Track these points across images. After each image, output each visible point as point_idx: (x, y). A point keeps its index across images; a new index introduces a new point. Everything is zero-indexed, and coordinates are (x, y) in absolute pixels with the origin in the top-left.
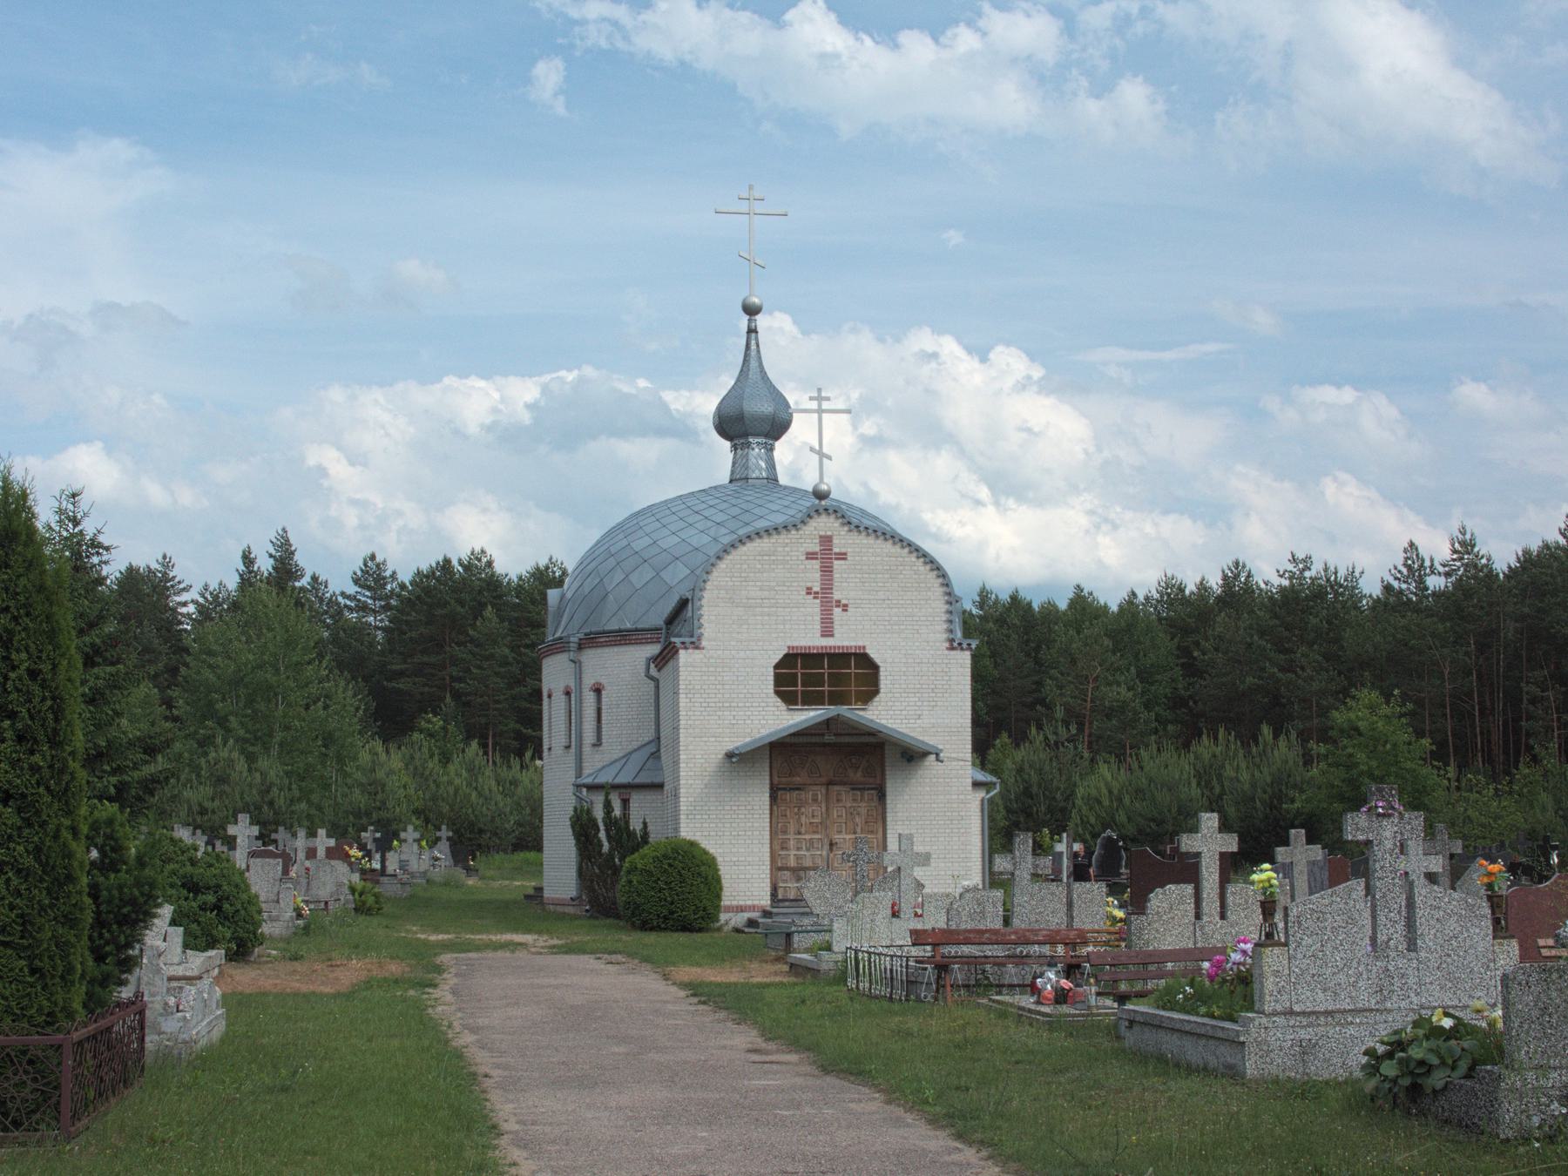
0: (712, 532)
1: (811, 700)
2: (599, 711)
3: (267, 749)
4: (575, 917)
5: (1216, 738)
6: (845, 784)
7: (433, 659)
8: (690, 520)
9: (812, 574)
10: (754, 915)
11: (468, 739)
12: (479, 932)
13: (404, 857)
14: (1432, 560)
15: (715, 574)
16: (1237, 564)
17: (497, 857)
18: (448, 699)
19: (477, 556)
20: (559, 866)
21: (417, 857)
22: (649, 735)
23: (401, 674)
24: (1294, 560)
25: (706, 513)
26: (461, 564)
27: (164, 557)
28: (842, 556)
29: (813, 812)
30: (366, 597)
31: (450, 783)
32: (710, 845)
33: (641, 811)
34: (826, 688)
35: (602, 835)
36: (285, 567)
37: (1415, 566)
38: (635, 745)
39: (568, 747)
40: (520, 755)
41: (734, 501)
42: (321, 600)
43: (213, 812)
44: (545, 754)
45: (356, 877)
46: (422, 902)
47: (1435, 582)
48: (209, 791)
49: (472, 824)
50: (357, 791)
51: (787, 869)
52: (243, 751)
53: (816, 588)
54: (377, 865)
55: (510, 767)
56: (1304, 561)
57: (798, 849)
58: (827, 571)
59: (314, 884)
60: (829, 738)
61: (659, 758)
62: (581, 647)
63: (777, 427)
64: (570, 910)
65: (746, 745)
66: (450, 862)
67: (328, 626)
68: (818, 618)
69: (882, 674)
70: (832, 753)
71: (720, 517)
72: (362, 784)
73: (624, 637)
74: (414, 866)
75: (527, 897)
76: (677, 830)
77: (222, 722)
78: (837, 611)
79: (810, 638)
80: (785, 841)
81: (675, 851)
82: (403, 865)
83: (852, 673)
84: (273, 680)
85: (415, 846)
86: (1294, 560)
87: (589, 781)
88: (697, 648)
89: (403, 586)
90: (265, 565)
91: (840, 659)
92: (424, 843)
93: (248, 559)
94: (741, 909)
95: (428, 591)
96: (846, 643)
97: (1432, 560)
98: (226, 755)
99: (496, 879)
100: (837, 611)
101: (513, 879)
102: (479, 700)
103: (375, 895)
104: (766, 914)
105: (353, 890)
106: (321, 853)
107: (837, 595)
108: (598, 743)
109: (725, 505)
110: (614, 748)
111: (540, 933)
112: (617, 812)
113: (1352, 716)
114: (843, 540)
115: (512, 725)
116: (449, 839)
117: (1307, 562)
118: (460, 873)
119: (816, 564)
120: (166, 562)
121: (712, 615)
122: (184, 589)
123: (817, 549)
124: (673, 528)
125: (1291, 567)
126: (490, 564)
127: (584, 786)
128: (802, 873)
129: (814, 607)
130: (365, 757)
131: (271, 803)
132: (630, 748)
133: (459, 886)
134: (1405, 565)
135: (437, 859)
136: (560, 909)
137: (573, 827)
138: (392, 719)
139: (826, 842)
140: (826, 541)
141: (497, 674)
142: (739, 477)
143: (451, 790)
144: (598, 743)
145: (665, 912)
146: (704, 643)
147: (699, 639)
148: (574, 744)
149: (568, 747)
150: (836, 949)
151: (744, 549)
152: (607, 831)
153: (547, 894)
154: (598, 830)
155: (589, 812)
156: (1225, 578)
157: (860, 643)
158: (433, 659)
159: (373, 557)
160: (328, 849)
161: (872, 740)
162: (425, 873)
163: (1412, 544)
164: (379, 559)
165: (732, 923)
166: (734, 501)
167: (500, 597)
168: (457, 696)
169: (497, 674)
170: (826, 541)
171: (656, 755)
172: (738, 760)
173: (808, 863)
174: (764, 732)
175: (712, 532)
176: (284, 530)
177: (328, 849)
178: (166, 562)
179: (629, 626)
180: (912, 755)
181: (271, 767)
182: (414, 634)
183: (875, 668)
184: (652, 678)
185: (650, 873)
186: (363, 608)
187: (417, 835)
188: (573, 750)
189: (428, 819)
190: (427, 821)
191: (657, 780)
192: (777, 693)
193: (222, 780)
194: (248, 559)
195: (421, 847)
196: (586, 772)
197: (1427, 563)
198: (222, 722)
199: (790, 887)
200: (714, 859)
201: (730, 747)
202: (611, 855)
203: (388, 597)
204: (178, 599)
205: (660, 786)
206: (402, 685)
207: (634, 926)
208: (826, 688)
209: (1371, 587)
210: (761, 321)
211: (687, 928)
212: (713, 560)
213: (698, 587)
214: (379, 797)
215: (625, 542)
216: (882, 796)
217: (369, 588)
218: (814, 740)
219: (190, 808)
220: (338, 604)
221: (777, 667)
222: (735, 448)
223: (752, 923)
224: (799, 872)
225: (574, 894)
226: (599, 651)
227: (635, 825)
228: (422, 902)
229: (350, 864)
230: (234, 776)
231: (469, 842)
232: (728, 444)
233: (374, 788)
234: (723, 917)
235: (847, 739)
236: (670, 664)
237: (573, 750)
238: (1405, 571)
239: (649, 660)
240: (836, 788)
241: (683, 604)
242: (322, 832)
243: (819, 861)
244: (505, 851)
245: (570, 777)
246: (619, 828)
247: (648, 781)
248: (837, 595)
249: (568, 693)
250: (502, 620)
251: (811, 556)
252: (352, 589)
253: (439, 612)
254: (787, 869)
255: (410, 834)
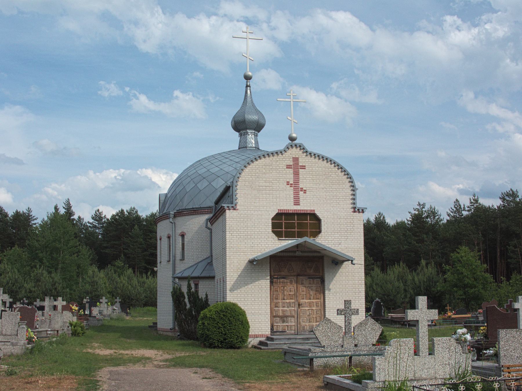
0: (234, 166)
1: (289, 235)
2: (183, 245)
3: (56, 269)
4: (172, 339)
5: (399, 265)
6: (305, 276)
7: (117, 242)
8: (224, 161)
9: (289, 175)
10: (263, 339)
11: (129, 267)
12: (127, 349)
13: (101, 309)
14: (464, 205)
15: (243, 174)
16: (380, 214)
17: (138, 308)
18: (122, 256)
19: (133, 209)
20: (165, 315)
21: (105, 310)
22: (207, 254)
23: (106, 248)
24: (419, 204)
25: (231, 158)
26: (127, 212)
27: (29, 208)
28: (303, 167)
29: (290, 288)
30: (96, 223)
31: (121, 282)
32: (242, 306)
33: (204, 290)
34: (296, 230)
35: (186, 300)
36: (69, 212)
37: (458, 207)
38: (200, 260)
39: (169, 261)
40: (146, 273)
41: (243, 154)
42: (82, 224)
43: (34, 292)
44: (158, 265)
45: (75, 319)
46: (103, 328)
47: (465, 213)
48: (33, 285)
49: (129, 297)
50: (87, 285)
51: (278, 316)
52: (47, 271)
53: (292, 182)
54: (87, 312)
55: (142, 277)
56: (423, 205)
57: (283, 307)
58: (296, 174)
59: (53, 322)
60: (298, 254)
61: (212, 265)
62: (175, 216)
63: (258, 127)
64: (170, 334)
65: (259, 256)
66: (120, 311)
67: (83, 233)
68: (292, 196)
69: (323, 223)
70: (300, 261)
71: (237, 160)
72: (89, 282)
73: (195, 212)
74: (105, 312)
75: (150, 327)
76: (224, 297)
77: (41, 261)
78: (301, 193)
79: (289, 206)
80: (277, 303)
81: (226, 308)
82: (100, 313)
83: (309, 222)
84: (59, 246)
85: (106, 304)
86: (419, 204)
87: (179, 275)
88: (234, 209)
89: (108, 220)
90: (62, 211)
91: (302, 215)
92: (109, 304)
93: (56, 208)
94: (256, 336)
95: (116, 220)
96: (305, 209)
97: (464, 205)
98: (40, 271)
99: (138, 319)
100: (301, 193)
101: (143, 317)
102: (133, 256)
103: (81, 327)
104: (268, 338)
105: (71, 324)
106: (60, 308)
107: (301, 186)
108: (183, 259)
109: (239, 155)
110: (190, 261)
111: (158, 349)
112: (193, 290)
113: (459, 256)
114: (303, 160)
115: (143, 264)
116: (120, 302)
117: (424, 205)
118: (124, 315)
119: (291, 171)
120: (29, 210)
121: (242, 194)
122: (35, 219)
123: (292, 163)
124: (216, 164)
125: (418, 207)
126: (137, 212)
127: (177, 278)
128: (285, 319)
129: (290, 191)
130: (90, 272)
131: (56, 289)
132: (198, 261)
133: (123, 320)
134: (455, 207)
135: (115, 310)
136: (165, 333)
137: (173, 297)
138: (102, 262)
139: (297, 303)
140: (296, 160)
141: (138, 248)
142: (243, 146)
143: (122, 285)
144: (183, 259)
145: (222, 339)
146: (238, 207)
147: (236, 205)
148: (172, 260)
149: (169, 261)
150: (377, 379)
151: (257, 162)
152: (189, 298)
153: (159, 326)
154: (185, 298)
155: (180, 289)
156: (376, 218)
157: (312, 209)
158: (117, 242)
159: (98, 210)
160: (63, 306)
161: (316, 254)
162: (110, 315)
163: (457, 200)
164: (100, 211)
165: (252, 343)
166: (243, 154)
167: (140, 222)
168: (125, 255)
169: (138, 248)
170: (296, 160)
171: (210, 264)
172: (254, 264)
173: (288, 314)
174: (267, 250)
175: (234, 166)
176: (68, 199)
177: (63, 306)
178: (29, 210)
179: (197, 206)
180: (337, 261)
181: (57, 277)
182: (111, 234)
183: (319, 220)
184: (209, 229)
185: (214, 320)
186: (95, 227)
187: (107, 301)
188: (171, 262)
189: (112, 295)
190: (113, 296)
191: (212, 275)
192: (273, 231)
193: (39, 280)
194: (56, 208)
195: (108, 305)
196: (177, 272)
197: (462, 207)
198: (41, 261)
199: (280, 325)
200: (244, 312)
201: (251, 257)
202: (190, 310)
203: (103, 224)
204: (33, 222)
205: (213, 278)
206: (107, 251)
207: (205, 346)
208: (296, 230)
209: (444, 215)
210: (251, 83)
211: (232, 347)
212: (243, 167)
213: (235, 178)
214: (95, 287)
215: (195, 171)
216: (323, 281)
217: (97, 220)
218: (291, 254)
219: (26, 291)
220: (87, 226)
221: (273, 219)
222: (241, 135)
223: (261, 343)
224: (284, 318)
225: (171, 326)
226: (183, 218)
227: (202, 295)
228: (103, 328)
229: (73, 313)
230: (42, 279)
231: (127, 304)
232: (238, 134)
233: (93, 283)
234: (249, 340)
235: (306, 254)
236: (220, 219)
237: (171, 262)
238: (455, 209)
239: (207, 220)
240: (301, 277)
241: (227, 189)
242: (60, 299)
243: (293, 313)
244: (141, 307)
245: (170, 274)
246: (194, 296)
247: (208, 275)
248: (301, 186)
249: (169, 237)
250: (140, 230)
251: (289, 167)
252: (91, 221)
253: (119, 227)
254: (278, 316)
255: (104, 300)
